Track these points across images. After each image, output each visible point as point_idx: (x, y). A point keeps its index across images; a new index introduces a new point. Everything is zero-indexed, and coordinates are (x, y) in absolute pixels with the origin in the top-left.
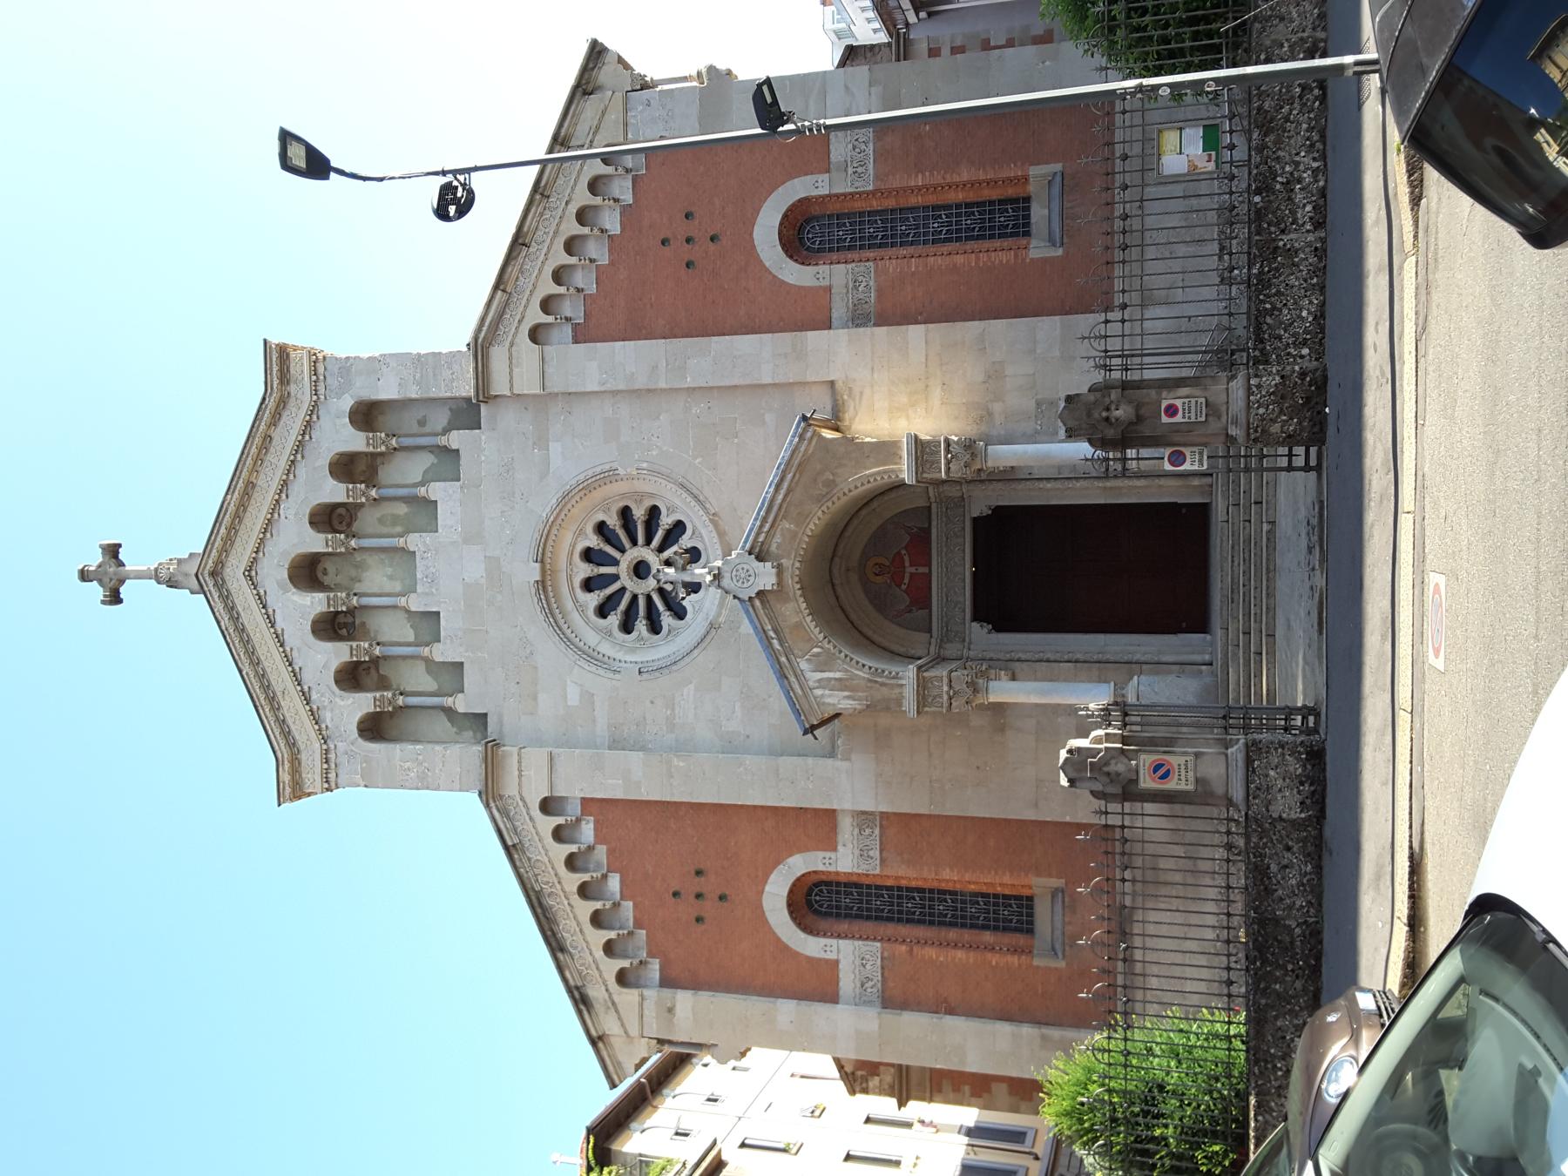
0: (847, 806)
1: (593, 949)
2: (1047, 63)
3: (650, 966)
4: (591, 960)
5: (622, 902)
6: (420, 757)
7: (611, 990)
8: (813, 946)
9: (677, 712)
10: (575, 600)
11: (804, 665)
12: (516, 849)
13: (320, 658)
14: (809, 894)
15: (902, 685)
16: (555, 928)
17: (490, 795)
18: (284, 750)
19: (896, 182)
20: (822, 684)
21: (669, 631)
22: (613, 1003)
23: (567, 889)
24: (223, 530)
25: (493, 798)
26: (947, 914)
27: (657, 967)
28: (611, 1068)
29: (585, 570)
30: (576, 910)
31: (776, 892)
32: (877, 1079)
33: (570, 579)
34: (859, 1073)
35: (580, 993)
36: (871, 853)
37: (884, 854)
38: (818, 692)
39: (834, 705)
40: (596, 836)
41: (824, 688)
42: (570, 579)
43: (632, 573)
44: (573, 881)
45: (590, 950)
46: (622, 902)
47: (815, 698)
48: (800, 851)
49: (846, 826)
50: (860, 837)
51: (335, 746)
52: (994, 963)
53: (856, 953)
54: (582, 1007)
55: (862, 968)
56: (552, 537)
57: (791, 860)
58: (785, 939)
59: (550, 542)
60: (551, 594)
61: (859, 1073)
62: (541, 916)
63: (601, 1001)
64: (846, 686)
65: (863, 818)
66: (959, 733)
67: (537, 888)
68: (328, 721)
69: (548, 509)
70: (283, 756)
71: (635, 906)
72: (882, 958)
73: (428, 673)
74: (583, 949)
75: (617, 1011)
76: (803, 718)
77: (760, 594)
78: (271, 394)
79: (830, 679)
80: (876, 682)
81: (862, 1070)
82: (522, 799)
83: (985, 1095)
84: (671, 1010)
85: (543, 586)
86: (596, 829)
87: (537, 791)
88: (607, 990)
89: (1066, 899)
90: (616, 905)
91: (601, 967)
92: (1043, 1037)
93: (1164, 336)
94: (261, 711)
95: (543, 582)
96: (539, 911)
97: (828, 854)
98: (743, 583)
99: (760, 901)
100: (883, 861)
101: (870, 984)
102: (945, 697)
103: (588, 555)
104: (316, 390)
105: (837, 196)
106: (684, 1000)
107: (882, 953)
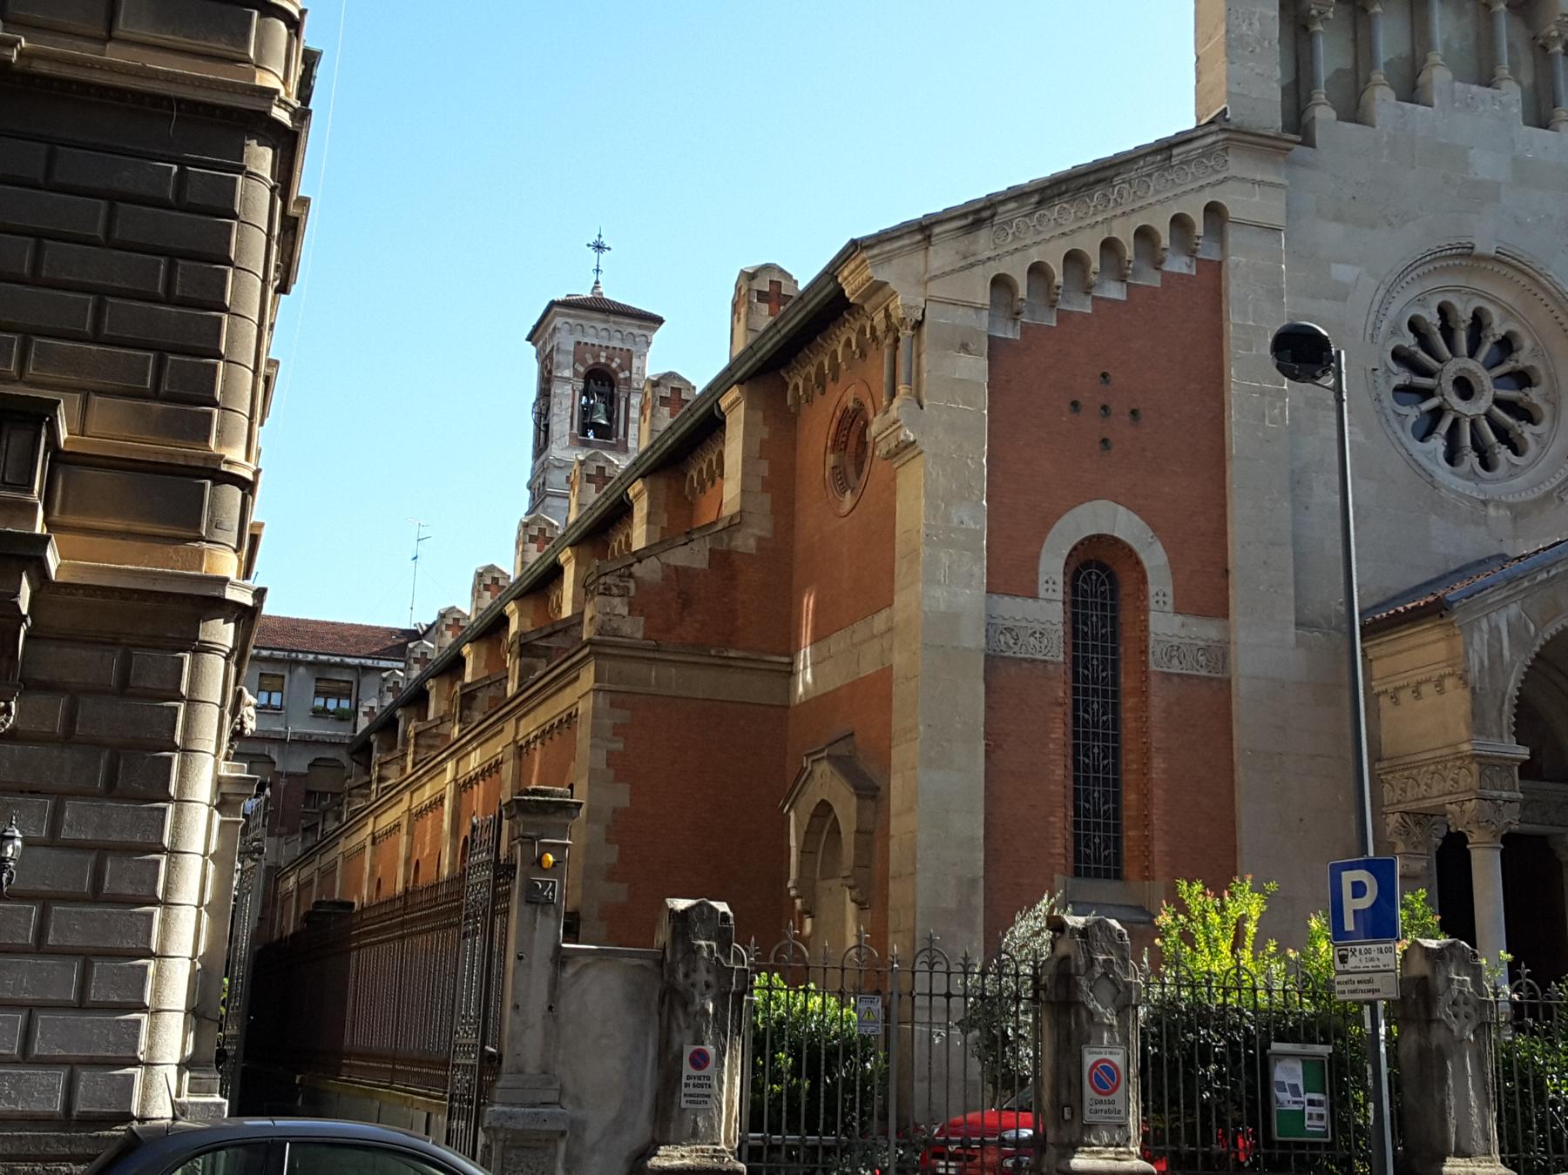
1: (1041, 247)
3: (1010, 324)
4: (1028, 241)
5: (1090, 297)
6: (1266, 44)
8: (1052, 566)
10: (1432, 292)
11: (1514, 609)
12: (1165, 160)
14: (1102, 567)
15: (1501, 736)
16: (1066, 197)
19: (1157, 702)
20: (1494, 631)
21: (1399, 415)
22: (972, 265)
23: (1115, 223)
26: (1088, 757)
28: (887, 247)
29: (1464, 311)
30: (1088, 231)
31: (1122, 523)
32: (625, 611)
33: (1456, 290)
34: (632, 585)
35: (985, 220)
36: (1175, 661)
37: (1176, 679)
38: (1485, 626)
40: (1173, 274)
41: (1490, 632)
42: (1456, 290)
43: (1467, 376)
44: (1125, 234)
45: (1039, 243)
46: (1090, 297)
47: (1478, 620)
49: (1208, 630)
50: (1195, 648)
52: (1052, 819)
53: (1048, 626)
54: (970, 219)
55: (1030, 632)
56: (1518, 277)
57: (1159, 547)
58: (1058, 525)
59: (1511, 273)
60: (1451, 263)
61: (632, 585)
62: (1085, 180)
65: (1220, 654)
66: (1340, 798)
67: (1117, 180)
69: (1557, 279)
71: (1085, 315)
72: (1046, 661)
73: (1337, 71)
74: (1039, 232)
75: (963, 269)
79: (1500, 641)
80: (1503, 704)
81: (637, 588)
82: (1225, 179)
83: (611, 772)
84: (964, 347)
85: (1466, 254)
86: (1180, 275)
87: (1237, 204)
88: (989, 259)
89: (1142, 926)
90: (1087, 289)
91: (1018, 255)
92: (974, 881)
93: (945, 1057)
95: (1469, 255)
96: (1092, 178)
97: (1170, 601)
100: (1168, 676)
101: (1011, 642)
102: (1495, 793)
103: (1478, 322)
106: (975, 368)
107: (1052, 662)
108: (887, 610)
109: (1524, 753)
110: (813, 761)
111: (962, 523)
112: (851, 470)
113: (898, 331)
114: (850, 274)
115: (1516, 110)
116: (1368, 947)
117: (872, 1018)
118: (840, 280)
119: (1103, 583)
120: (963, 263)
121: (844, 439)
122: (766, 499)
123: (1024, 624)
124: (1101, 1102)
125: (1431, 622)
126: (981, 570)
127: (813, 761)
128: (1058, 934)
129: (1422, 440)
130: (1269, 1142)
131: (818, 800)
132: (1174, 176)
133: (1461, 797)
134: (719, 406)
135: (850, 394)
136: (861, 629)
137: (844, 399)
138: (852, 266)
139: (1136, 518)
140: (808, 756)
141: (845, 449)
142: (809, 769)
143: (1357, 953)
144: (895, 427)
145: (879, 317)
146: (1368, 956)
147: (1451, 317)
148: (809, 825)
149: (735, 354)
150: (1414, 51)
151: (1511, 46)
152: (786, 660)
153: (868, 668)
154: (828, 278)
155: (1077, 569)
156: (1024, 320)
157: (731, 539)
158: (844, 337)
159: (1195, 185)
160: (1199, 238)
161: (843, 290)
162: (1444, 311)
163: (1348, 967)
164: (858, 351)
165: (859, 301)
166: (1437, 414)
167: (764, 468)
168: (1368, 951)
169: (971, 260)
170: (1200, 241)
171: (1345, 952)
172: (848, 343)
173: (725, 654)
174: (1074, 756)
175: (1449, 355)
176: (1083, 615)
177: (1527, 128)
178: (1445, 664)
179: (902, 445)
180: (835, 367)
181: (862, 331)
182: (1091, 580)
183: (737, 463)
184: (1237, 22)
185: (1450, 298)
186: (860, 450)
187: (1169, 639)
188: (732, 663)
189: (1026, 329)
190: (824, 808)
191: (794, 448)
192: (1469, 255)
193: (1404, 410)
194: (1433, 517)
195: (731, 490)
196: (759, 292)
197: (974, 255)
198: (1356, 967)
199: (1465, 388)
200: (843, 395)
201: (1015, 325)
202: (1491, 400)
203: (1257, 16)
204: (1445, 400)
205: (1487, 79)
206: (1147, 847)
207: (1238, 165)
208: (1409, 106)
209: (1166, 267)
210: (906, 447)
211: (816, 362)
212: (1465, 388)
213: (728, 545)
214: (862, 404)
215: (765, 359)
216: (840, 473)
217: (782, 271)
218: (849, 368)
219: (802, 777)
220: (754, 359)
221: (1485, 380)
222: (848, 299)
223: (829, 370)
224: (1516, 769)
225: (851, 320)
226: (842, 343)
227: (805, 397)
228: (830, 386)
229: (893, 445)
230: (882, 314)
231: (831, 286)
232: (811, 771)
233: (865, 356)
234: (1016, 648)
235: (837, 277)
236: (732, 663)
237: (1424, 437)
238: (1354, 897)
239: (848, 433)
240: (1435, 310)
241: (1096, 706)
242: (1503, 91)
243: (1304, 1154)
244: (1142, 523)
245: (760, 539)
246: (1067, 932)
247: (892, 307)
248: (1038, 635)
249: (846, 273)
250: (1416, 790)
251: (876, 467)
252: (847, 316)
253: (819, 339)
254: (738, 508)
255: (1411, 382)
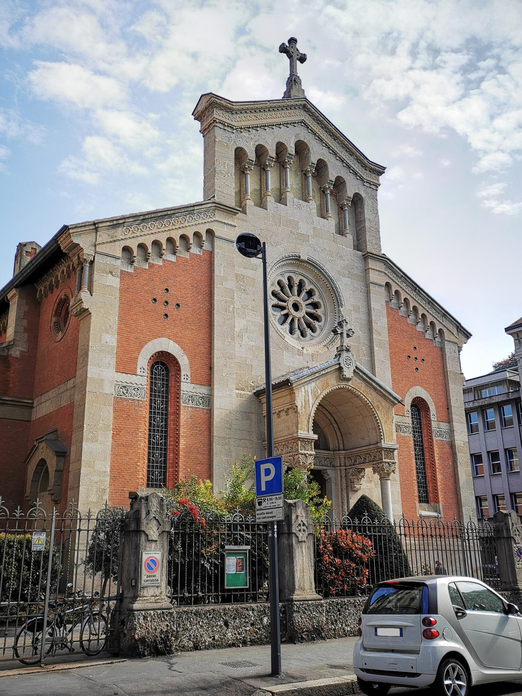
0: (216, 393)
2: (472, 513)
3: (130, 266)
4: (138, 234)
6: (230, 175)
7: (121, 242)
9: (251, 312)
13: (270, 141)
17: (217, 205)
18: (370, 165)
21: (274, 315)
24: (322, 119)
25: (216, 206)
27: (129, 271)
36: (190, 402)
39: (298, 396)
40: (194, 254)
41: (305, 392)
47: (300, 388)
48: (191, 363)
50: (198, 397)
51: (234, 133)
52: (138, 464)
53: (140, 386)
55: (133, 388)
57: (185, 357)
63: (115, 234)
64: (306, 404)
68: (245, 134)
70: (233, 105)
71: (160, 266)
72: (139, 400)
76: (297, 380)
77: (340, 369)
78: (368, 163)
92: (105, 490)
94: (252, 103)
98: (345, 362)
99: (165, 336)
101: (125, 392)
102: (306, 452)
104: (229, 126)
105: (430, 424)
106: (115, 282)
108: (74, 379)
109: (316, 437)
110: (39, 443)
111: (107, 343)
112: (62, 324)
113: (83, 264)
114: (63, 240)
115: (315, 211)
116: (271, 497)
117: (40, 542)
118: (59, 242)
119: (163, 371)
120: (111, 240)
121: (60, 311)
122: (26, 335)
123: (130, 385)
124: (150, 576)
125: (284, 388)
126: (113, 362)
127: (39, 443)
128: (134, 500)
129: (281, 325)
130: (223, 590)
131: (40, 458)
132: (195, 217)
133: (294, 453)
134: (7, 297)
135: (63, 293)
136: (63, 387)
137: (60, 295)
138: (64, 236)
139: (177, 346)
140: (37, 440)
141: (60, 316)
142: (37, 446)
143: (266, 501)
144: (80, 302)
145: (75, 259)
146: (271, 501)
147: (292, 282)
148: (36, 469)
149: (15, 274)
150: (280, 186)
151: (313, 190)
152: (31, 402)
153: (64, 404)
154: (54, 241)
155: (153, 364)
156: (135, 265)
157: (8, 351)
158: (62, 268)
159: (203, 221)
160: (204, 241)
161: (60, 247)
162: (290, 279)
163: (262, 507)
164: (66, 275)
165: (67, 252)
166: (286, 316)
167: (25, 323)
168: (271, 499)
169: (115, 239)
170: (204, 243)
171: (261, 500)
172: (63, 272)
173: (3, 398)
174: (149, 438)
175: (291, 295)
176: (155, 382)
177: (318, 218)
178: (289, 404)
179: (82, 310)
180: (57, 282)
181: (69, 267)
182: (158, 369)
183: (13, 320)
184: (219, 165)
185: (292, 275)
186: (66, 317)
187: (188, 393)
188: (6, 402)
189: (135, 269)
190: (43, 462)
191: (39, 316)
192: (298, 260)
193: (275, 313)
194: (285, 352)
195: (10, 332)
196: (27, 252)
197: (116, 237)
198: (265, 507)
199: (296, 307)
200: (59, 294)
201: (131, 267)
202: (305, 312)
203: (226, 164)
204: (289, 311)
205: (306, 200)
206: (176, 475)
207: (219, 216)
208: (279, 204)
209: (191, 251)
210: (84, 311)
211: (49, 280)
212: (296, 307)
213: (8, 353)
214: (68, 297)
215: (27, 277)
216: (57, 325)
217: (36, 244)
218: (63, 282)
219: (34, 449)
220: (22, 277)
221: (303, 304)
222: (62, 251)
223: (55, 283)
224: (313, 443)
225: (64, 262)
226: (60, 271)
227: (44, 294)
228: (55, 289)
229: (78, 310)
230: (76, 258)
231: (56, 244)
232: (38, 447)
233: (70, 277)
234: (127, 395)
235: (58, 241)
236: (6, 402)
237: (283, 323)
238: (266, 476)
239: (62, 309)
240: (286, 279)
241: (158, 419)
242: (310, 204)
243: (244, 594)
244: (179, 347)
245: (21, 352)
246: (138, 500)
247: (80, 254)
248: (136, 390)
249: (62, 239)
250: (278, 452)
251: (72, 320)
252: (63, 261)
253: (51, 271)
254: (13, 339)
255: (278, 303)
